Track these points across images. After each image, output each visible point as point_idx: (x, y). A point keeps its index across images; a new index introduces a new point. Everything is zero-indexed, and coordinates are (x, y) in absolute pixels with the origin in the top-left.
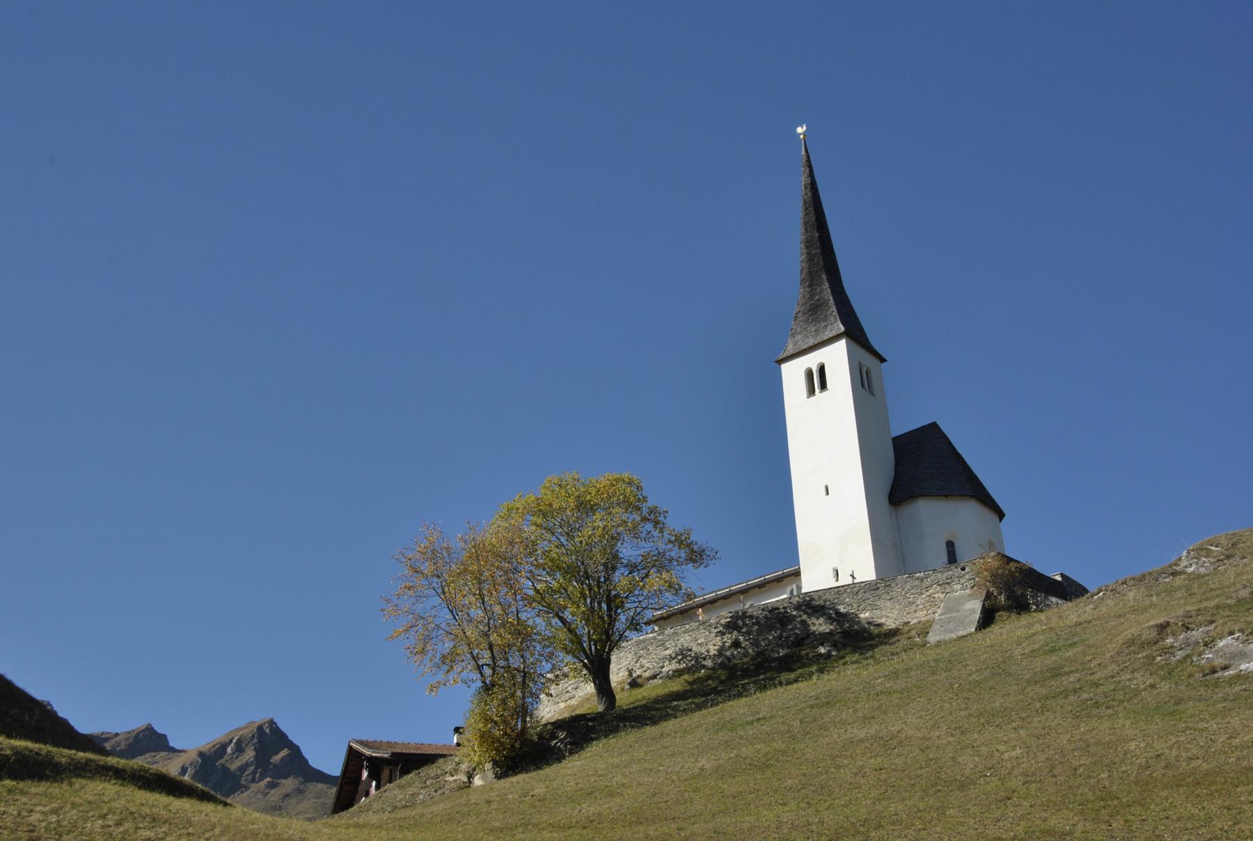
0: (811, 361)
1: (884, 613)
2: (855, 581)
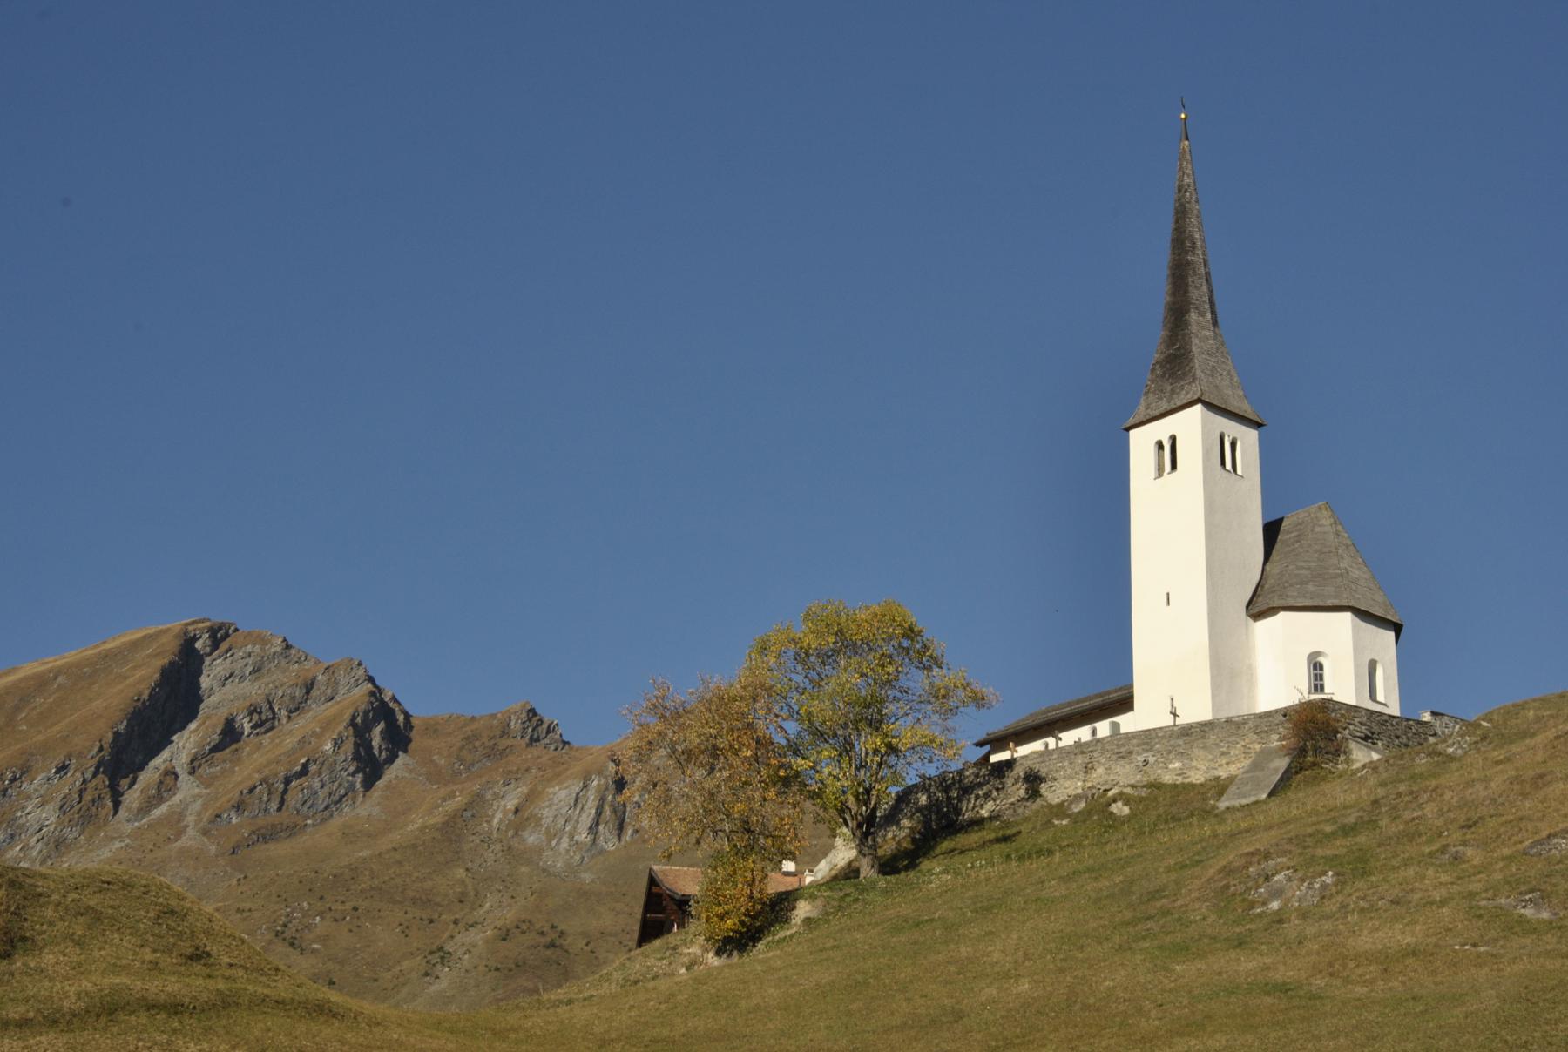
0: (1160, 429)
1: (1194, 763)
2: (1179, 721)
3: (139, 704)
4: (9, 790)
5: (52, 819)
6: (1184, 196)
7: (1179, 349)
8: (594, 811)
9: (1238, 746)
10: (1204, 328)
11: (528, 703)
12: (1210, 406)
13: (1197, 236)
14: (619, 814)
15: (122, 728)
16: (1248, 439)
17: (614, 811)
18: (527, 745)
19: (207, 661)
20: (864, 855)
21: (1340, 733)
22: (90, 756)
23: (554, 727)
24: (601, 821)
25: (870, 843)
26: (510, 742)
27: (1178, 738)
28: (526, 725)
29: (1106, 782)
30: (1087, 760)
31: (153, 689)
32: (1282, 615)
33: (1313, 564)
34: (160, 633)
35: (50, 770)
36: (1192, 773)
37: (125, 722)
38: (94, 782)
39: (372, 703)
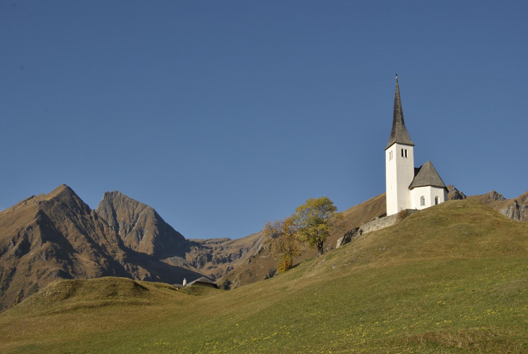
8: (512, 214)
10: (399, 125)
12: (397, 143)
13: (399, 104)
14: (518, 214)
16: (410, 150)
17: (517, 213)
19: (14, 254)
24: (514, 216)
25: (321, 249)
26: (490, 200)
32: (415, 189)
33: (423, 176)
39: (456, 195)
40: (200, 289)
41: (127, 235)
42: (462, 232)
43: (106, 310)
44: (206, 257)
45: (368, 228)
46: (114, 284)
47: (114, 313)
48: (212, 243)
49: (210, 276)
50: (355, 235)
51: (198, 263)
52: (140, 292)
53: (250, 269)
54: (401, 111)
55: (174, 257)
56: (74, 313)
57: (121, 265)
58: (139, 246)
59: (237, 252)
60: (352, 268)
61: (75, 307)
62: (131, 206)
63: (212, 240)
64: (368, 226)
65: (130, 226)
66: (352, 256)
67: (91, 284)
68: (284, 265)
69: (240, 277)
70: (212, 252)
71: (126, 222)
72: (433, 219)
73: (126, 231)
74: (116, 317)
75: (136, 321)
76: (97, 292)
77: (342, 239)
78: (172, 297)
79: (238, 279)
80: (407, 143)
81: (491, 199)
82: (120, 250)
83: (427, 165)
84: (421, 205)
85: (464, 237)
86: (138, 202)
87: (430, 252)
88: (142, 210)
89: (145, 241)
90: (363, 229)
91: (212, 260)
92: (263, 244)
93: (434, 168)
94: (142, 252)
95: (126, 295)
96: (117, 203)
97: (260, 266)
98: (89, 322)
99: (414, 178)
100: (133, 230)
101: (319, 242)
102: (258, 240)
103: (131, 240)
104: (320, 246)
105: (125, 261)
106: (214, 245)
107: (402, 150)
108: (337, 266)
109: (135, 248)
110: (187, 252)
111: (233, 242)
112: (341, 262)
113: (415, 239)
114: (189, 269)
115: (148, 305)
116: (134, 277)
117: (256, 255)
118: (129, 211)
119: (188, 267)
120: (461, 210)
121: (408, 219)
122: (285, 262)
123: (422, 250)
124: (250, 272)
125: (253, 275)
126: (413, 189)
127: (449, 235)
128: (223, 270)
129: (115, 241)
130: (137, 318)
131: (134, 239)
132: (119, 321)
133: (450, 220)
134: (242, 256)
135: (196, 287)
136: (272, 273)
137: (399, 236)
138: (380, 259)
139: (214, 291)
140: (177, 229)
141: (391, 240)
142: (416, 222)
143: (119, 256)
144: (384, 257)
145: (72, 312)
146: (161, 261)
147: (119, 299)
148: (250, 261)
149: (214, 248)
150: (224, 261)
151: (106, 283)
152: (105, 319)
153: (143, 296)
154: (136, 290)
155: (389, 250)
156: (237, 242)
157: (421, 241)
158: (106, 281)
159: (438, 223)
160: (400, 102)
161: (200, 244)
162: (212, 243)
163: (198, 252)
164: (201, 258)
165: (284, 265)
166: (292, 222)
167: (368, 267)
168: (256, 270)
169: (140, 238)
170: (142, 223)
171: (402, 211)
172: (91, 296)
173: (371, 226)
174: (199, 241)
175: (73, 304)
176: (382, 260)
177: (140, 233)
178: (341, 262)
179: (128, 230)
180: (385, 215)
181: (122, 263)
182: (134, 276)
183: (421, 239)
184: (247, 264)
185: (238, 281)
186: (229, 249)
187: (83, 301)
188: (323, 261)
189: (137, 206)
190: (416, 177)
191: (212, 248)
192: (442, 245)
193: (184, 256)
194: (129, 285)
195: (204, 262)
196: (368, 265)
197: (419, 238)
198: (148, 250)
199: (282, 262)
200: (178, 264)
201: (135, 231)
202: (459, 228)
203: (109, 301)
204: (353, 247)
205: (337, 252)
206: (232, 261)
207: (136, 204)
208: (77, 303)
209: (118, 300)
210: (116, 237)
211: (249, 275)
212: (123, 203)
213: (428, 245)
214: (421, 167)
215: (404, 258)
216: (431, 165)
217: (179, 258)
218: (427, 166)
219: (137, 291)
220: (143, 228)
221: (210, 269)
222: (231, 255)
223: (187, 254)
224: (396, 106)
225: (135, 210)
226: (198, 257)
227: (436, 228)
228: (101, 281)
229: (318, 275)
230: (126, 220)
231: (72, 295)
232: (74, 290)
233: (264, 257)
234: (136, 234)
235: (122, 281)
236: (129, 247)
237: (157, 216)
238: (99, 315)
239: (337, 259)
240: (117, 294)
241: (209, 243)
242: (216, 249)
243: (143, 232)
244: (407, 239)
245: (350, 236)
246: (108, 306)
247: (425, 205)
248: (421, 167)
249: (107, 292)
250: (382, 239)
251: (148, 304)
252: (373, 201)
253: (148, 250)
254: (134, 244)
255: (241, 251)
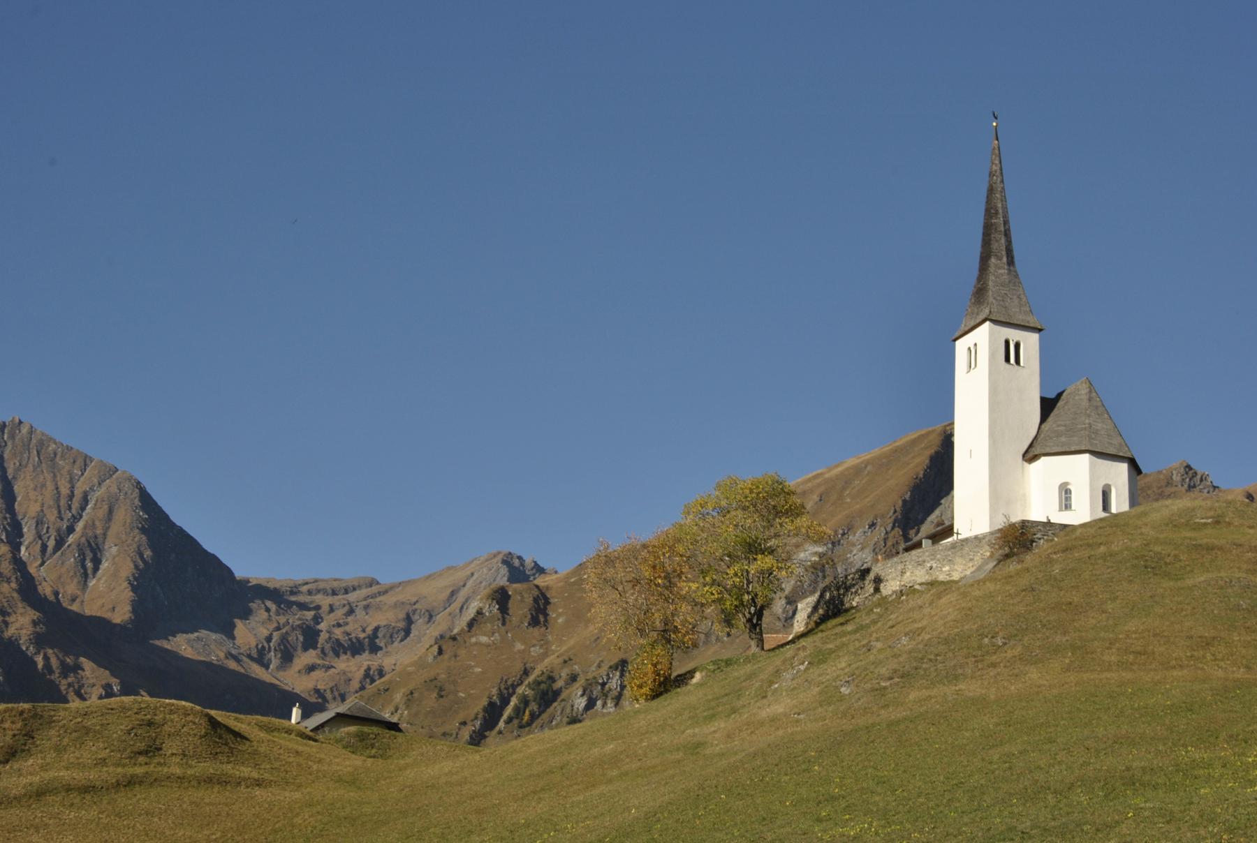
1: (956, 567)
3: (918, 481)
4: (842, 541)
5: (869, 558)
6: (992, 179)
7: (983, 284)
9: (979, 554)
11: (1184, 461)
12: (993, 321)
13: (1000, 205)
15: (907, 497)
16: (1030, 343)
18: (1187, 491)
20: (752, 639)
21: (1036, 542)
22: (889, 516)
23: (1206, 478)
25: (758, 630)
26: (1174, 489)
27: (949, 550)
28: (1184, 477)
29: (910, 582)
30: (903, 567)
31: (926, 471)
32: (1043, 459)
33: (1068, 422)
34: (928, 434)
35: (864, 527)
36: (953, 574)
37: (909, 493)
38: (893, 533)
40: (384, 740)
41: (48, 559)
42: (1232, 599)
43: (134, 800)
44: (299, 636)
45: (899, 573)
46: (149, 721)
47: (160, 808)
48: (318, 591)
49: (309, 692)
50: (856, 592)
51: (272, 653)
52: (226, 744)
53: (438, 674)
54: (1007, 227)
55: (197, 631)
56: (34, 806)
57: (27, 655)
58: (86, 596)
59: (398, 621)
60: (909, 693)
61: (35, 788)
62: (63, 468)
63: (319, 583)
64: (900, 567)
65: (58, 530)
66: (901, 659)
67: (80, 720)
68: (650, 675)
69: (409, 700)
70: (317, 619)
71: (45, 519)
72: (1137, 558)
73: (44, 548)
74: (170, 821)
75: (232, 836)
76: (102, 745)
77: (812, 599)
78: (320, 761)
79: (401, 706)
80: (1022, 324)
81: (1176, 486)
82: (24, 608)
83: (1078, 390)
84: (1061, 510)
85: (1238, 613)
86: (86, 456)
87: (1143, 657)
88: (100, 484)
89: (106, 581)
90: (883, 574)
91: (319, 646)
92: (481, 599)
93: (1101, 401)
94: (94, 614)
95: (187, 753)
96: (18, 458)
97: (471, 667)
98: (88, 836)
99: (1039, 428)
100: (67, 544)
101: (753, 609)
102: (464, 586)
103: (60, 577)
104: (755, 621)
105: (40, 641)
106: (326, 597)
107: (1007, 343)
108: (857, 686)
109: (73, 600)
110: (241, 618)
111: (386, 592)
112: (867, 674)
113: (1092, 615)
114: (246, 671)
115: (258, 785)
116: (67, 693)
117: (459, 634)
118: (56, 484)
119: (241, 665)
120: (1209, 531)
121: (1055, 553)
122: (652, 665)
123: (1118, 649)
124: (439, 684)
125: (447, 696)
126: (1035, 461)
127: (1194, 608)
128: (349, 675)
129: (10, 578)
130: (234, 825)
131: (72, 573)
132: (180, 834)
133: (1187, 563)
134: (411, 635)
135: (372, 733)
136: (505, 688)
137: (1042, 605)
138: (993, 672)
139: (427, 747)
140: (209, 545)
141: (1019, 616)
142: (1085, 563)
143: (18, 625)
144: (1001, 665)
145: (30, 806)
146: (158, 643)
147: (169, 767)
148: (440, 652)
149: (325, 608)
150: (355, 648)
151: (126, 717)
152: (134, 826)
153: (237, 756)
154: (217, 740)
155: (1015, 645)
156: (397, 590)
157: (1111, 622)
158: (124, 709)
159: (1153, 568)
160: (1004, 199)
161: (283, 595)
162: (318, 591)
163: (274, 617)
164: (284, 639)
165: (650, 675)
166: (674, 545)
167: (958, 692)
168: (459, 681)
169: (90, 572)
170: (97, 523)
171: (1010, 525)
172: (82, 755)
173: (910, 567)
174: (277, 586)
175: (29, 779)
176: (998, 674)
177: (92, 554)
178: (867, 674)
179: (51, 544)
180: (949, 531)
181: (27, 649)
182: (66, 689)
183: (1108, 615)
184: (430, 659)
185: (399, 712)
186: (371, 611)
187: (60, 769)
188: (802, 667)
189: (85, 470)
190: (1046, 426)
191: (318, 608)
192: (1176, 637)
193: (229, 631)
194: (194, 723)
195: (292, 650)
196: (957, 688)
197: (1103, 612)
198: (116, 610)
199: (643, 664)
200: (209, 654)
201: (74, 547)
202: (1222, 588)
203: (139, 770)
204: (894, 629)
205: (838, 642)
206: (381, 648)
207: (83, 464)
208: (42, 777)
209: (166, 770)
210: (11, 567)
211: (435, 695)
212: (37, 459)
213: (1134, 636)
214: (1060, 395)
215: (1068, 670)
216: (1090, 392)
217: (214, 636)
218: (1077, 392)
219: (218, 743)
220: (100, 540)
221: (309, 673)
222: (377, 629)
223: (238, 622)
224: (993, 211)
225: (78, 480)
226: (275, 634)
227: (1151, 586)
228: (108, 709)
229: (796, 710)
230: (45, 511)
231: (23, 751)
232: (30, 735)
233: (484, 639)
234: (79, 556)
235: (171, 712)
236: (52, 598)
237: (147, 501)
238: (116, 815)
239: (850, 665)
240: (160, 749)
241: (310, 593)
242: (332, 609)
243: (100, 550)
244: (1064, 614)
245: (842, 591)
246: (137, 786)
247: (1073, 508)
248: (1060, 395)
249: (131, 743)
250: (990, 611)
251: (259, 783)
252: (820, 480)
253: (114, 608)
254: (71, 588)
255: (409, 620)
